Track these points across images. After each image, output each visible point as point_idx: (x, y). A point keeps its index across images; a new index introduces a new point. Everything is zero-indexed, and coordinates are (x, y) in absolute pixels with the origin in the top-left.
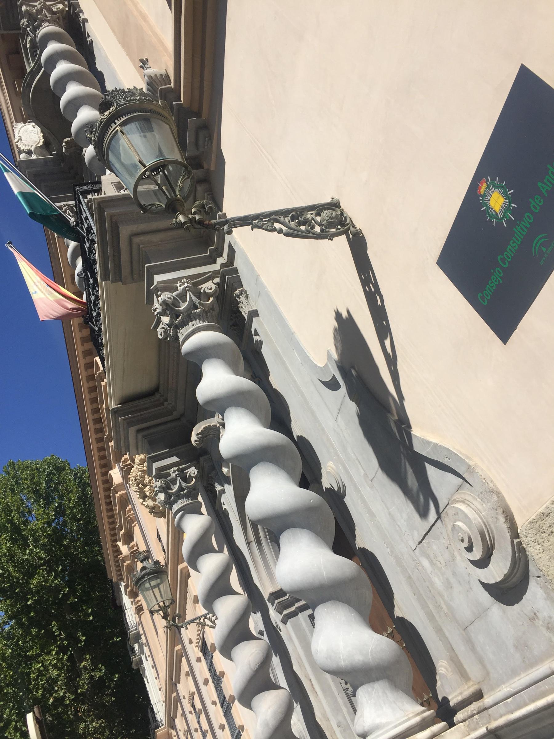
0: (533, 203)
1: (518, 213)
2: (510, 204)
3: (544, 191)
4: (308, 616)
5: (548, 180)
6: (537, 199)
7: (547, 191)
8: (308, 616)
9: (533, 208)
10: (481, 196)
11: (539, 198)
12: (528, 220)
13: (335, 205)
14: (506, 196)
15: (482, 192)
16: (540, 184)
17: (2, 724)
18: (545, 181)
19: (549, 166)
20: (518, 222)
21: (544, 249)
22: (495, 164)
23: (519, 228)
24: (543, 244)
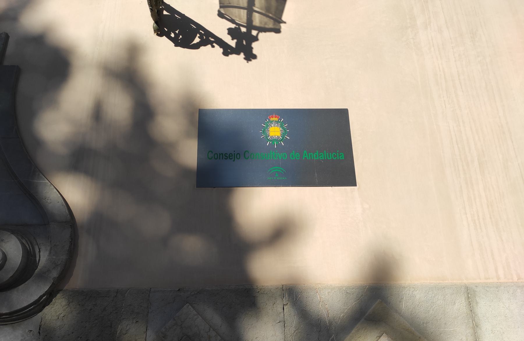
0: (294, 154)
1: (280, 149)
2: (281, 140)
3: (304, 156)
4: (342, 115)
5: (311, 155)
6: (285, 156)
7: (306, 158)
8: (342, 115)
9: (291, 155)
10: (269, 120)
11: (299, 156)
12: (282, 156)
13: (221, 15)
14: (283, 135)
15: (272, 119)
16: (305, 152)
17: (5, 311)
18: (309, 154)
19: (317, 151)
20: (277, 151)
21: (277, 175)
22: (290, 117)
23: (274, 154)
24: (278, 172)
